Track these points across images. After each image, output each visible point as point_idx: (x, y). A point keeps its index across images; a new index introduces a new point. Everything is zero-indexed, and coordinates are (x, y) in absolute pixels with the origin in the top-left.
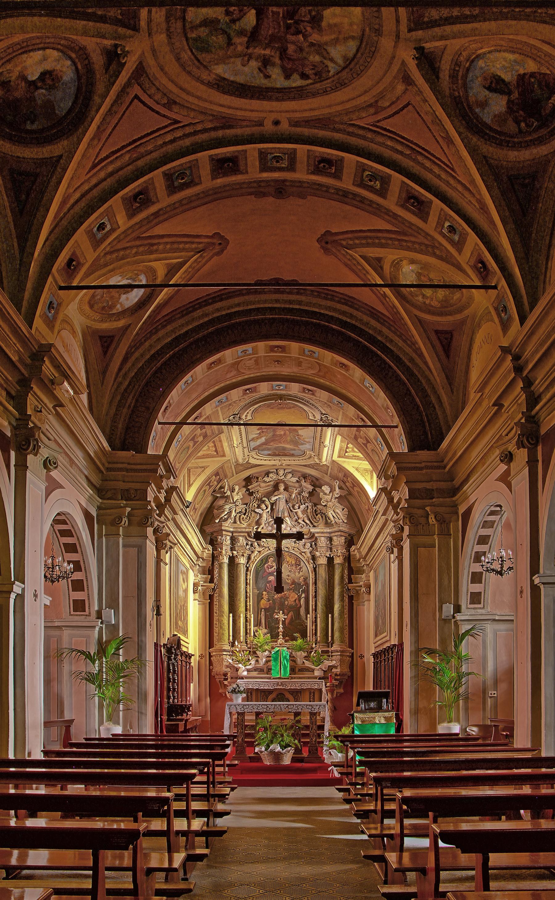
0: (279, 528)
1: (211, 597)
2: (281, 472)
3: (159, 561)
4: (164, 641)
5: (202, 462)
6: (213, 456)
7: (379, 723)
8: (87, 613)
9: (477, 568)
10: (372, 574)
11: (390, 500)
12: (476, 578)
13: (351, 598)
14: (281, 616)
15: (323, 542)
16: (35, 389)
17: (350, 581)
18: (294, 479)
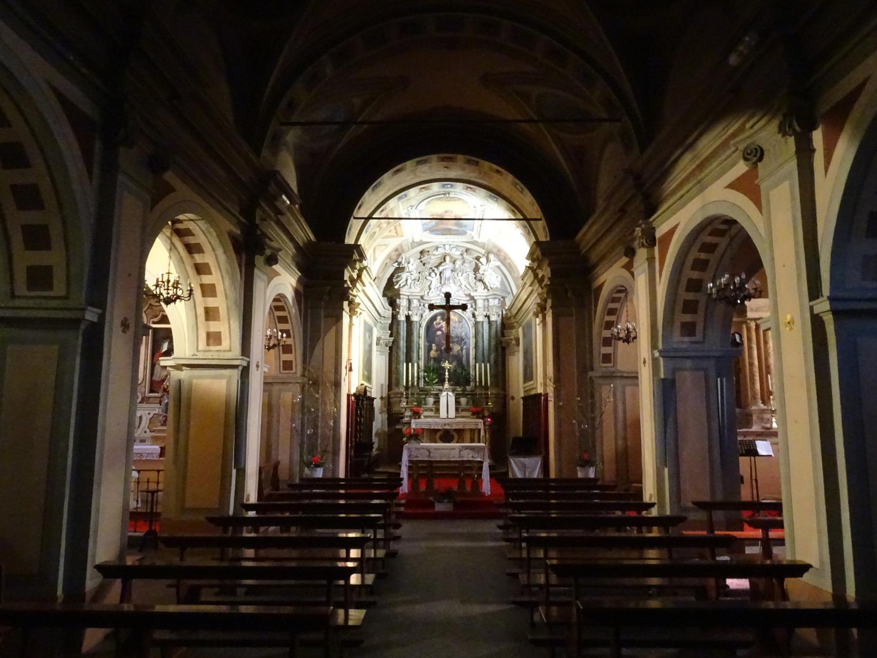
0: (448, 301)
1: (391, 348)
2: (447, 247)
3: (351, 325)
4: (353, 391)
5: (386, 241)
6: (393, 237)
7: (526, 467)
8: (294, 371)
9: (606, 334)
10: (520, 330)
11: (536, 275)
12: (607, 342)
13: (504, 349)
14: (446, 365)
15: (480, 303)
16: (263, 204)
17: (503, 335)
18: (459, 253)
